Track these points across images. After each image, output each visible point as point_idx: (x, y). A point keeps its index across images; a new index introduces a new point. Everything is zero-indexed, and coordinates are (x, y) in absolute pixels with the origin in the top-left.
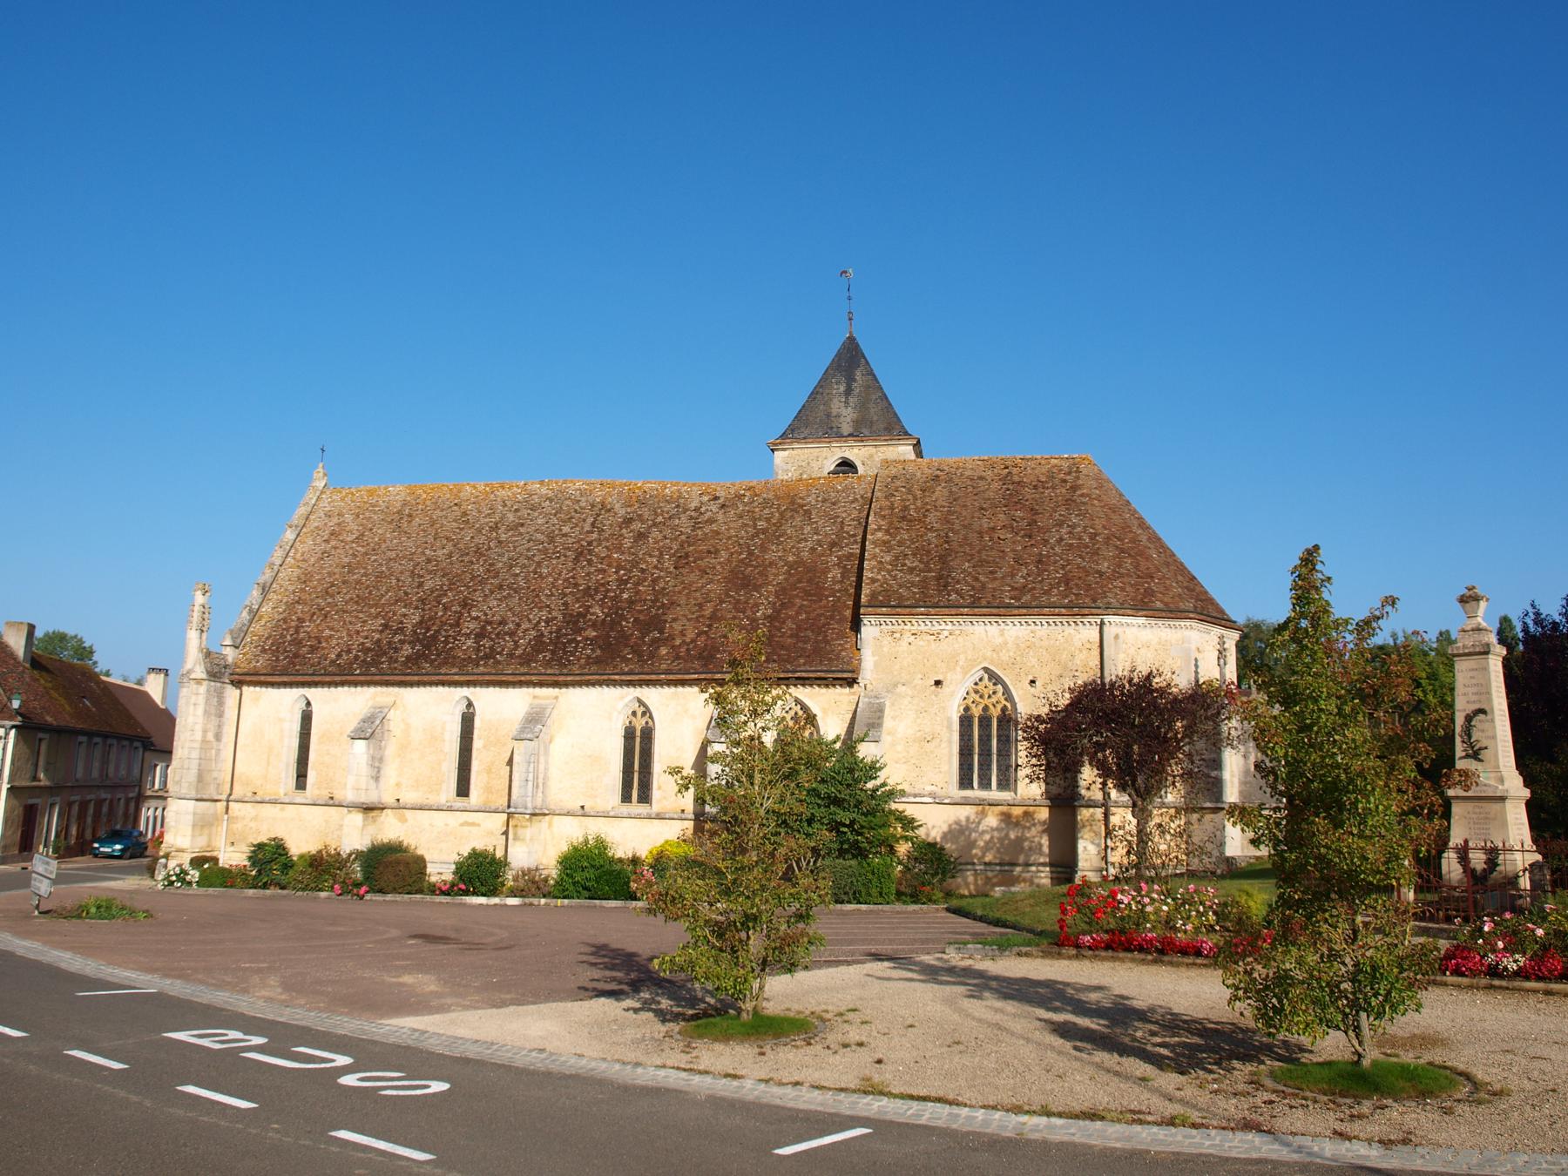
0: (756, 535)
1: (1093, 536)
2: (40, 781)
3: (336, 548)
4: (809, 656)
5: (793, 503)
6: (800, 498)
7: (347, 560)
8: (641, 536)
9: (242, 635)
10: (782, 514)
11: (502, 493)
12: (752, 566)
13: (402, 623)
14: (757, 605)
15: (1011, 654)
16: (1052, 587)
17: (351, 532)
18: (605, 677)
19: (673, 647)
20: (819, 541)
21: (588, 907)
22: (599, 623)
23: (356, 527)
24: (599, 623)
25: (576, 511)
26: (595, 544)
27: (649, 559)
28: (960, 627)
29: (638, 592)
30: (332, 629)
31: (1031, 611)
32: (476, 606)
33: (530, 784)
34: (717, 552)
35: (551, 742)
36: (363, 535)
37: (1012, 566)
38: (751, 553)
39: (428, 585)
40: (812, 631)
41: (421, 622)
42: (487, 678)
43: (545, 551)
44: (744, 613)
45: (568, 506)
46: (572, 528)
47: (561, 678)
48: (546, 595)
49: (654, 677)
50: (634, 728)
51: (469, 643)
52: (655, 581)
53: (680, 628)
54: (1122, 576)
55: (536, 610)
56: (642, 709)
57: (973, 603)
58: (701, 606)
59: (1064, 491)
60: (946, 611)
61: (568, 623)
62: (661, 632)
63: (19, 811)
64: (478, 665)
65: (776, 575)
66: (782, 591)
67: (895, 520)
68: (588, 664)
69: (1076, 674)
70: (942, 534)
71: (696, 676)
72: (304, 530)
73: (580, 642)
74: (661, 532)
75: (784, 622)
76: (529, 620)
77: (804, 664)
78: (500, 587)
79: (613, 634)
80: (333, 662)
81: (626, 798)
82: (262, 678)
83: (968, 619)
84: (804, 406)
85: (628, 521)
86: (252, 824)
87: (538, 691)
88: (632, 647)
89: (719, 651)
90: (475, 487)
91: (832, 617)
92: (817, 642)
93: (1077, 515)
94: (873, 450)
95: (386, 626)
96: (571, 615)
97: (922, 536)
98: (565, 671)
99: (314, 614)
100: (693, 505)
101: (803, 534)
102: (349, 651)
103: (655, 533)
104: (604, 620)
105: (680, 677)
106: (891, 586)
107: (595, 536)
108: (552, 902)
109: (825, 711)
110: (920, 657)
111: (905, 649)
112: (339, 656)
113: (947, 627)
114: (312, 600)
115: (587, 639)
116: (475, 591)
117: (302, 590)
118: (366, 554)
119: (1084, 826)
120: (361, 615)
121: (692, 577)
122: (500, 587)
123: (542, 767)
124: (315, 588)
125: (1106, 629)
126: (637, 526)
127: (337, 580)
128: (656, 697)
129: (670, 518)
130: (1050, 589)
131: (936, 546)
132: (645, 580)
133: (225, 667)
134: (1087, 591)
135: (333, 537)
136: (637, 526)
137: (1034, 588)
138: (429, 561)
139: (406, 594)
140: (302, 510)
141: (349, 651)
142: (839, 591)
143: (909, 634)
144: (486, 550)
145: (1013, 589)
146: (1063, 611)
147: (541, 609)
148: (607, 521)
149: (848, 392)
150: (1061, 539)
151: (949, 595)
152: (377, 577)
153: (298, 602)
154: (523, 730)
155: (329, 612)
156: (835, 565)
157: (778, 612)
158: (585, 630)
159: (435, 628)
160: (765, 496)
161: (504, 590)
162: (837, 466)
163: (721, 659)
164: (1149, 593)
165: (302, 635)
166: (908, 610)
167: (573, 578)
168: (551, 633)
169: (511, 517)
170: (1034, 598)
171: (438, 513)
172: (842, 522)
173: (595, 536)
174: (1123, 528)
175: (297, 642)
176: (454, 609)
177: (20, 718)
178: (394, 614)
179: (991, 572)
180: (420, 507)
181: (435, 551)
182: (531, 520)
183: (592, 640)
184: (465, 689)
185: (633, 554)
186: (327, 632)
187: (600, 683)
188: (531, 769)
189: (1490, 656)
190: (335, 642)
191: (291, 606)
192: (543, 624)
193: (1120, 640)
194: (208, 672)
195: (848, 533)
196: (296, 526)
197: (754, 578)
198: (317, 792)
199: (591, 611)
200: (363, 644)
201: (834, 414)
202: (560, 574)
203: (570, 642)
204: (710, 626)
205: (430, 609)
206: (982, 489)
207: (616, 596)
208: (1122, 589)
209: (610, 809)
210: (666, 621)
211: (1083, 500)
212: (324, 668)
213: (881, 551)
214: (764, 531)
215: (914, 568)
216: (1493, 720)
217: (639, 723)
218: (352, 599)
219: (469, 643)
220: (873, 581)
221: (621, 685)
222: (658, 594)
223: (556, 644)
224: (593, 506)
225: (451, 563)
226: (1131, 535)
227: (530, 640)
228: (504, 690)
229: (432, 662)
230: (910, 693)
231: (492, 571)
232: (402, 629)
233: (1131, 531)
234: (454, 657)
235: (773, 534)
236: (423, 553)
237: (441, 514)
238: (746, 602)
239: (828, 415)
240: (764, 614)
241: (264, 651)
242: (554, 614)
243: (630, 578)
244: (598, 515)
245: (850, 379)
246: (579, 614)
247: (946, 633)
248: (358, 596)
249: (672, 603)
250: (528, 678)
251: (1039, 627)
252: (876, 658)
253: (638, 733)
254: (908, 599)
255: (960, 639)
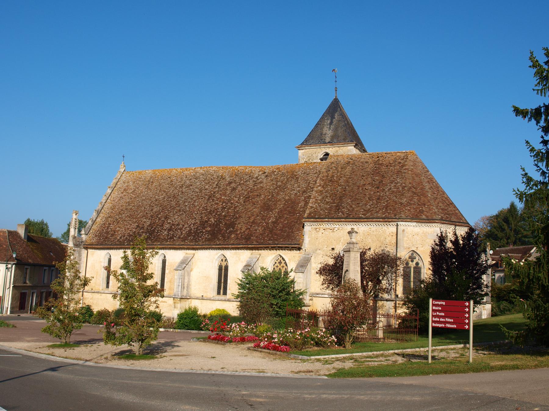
0: (276, 188)
1: (403, 188)
2: (27, 284)
3: (125, 195)
4: (284, 238)
5: (293, 174)
6: (296, 172)
7: (128, 200)
8: (234, 189)
9: (89, 230)
10: (288, 179)
11: (186, 172)
12: (272, 201)
13: (143, 225)
14: (270, 217)
15: (361, 237)
16: (380, 209)
17: (131, 189)
18: (210, 246)
19: (236, 234)
20: (299, 190)
21: (186, 332)
22: (212, 225)
23: (133, 187)
24: (212, 225)
25: (211, 179)
26: (216, 193)
27: (235, 199)
28: (342, 227)
29: (228, 212)
30: (119, 227)
31: (368, 220)
32: (170, 218)
33: (180, 287)
34: (261, 195)
35: (191, 271)
36: (135, 190)
37: (367, 201)
38: (273, 196)
39: (155, 210)
40: (288, 228)
41: (150, 225)
42: (169, 246)
43: (197, 196)
44: (264, 220)
45: (209, 177)
46: (209, 186)
47: (195, 247)
48: (195, 214)
49: (227, 246)
50: (222, 265)
51: (166, 233)
52: (235, 208)
53: (240, 227)
54: (411, 204)
55: (191, 220)
56: (225, 258)
57: (347, 216)
58: (249, 218)
59: (398, 167)
60: (336, 220)
61: (201, 225)
62: (233, 228)
63: (18, 295)
64: (167, 241)
65: (280, 205)
66: (281, 211)
67: (327, 181)
68: (205, 241)
69: (387, 246)
70: (344, 187)
71: (242, 246)
72: (115, 189)
73: (204, 232)
74: (241, 187)
75: (278, 224)
76: (188, 224)
77: (282, 241)
78: (180, 211)
79: (216, 229)
80: (118, 240)
81: (219, 293)
82: (94, 246)
83: (345, 223)
84: (312, 130)
85: (230, 183)
86: (91, 301)
87: (188, 251)
88: (222, 234)
89: (252, 236)
90: (177, 170)
91: (297, 222)
92: (289, 232)
93: (400, 178)
94: (338, 149)
95: (138, 226)
96: (203, 222)
97: (336, 188)
98: (197, 244)
99: (114, 221)
100: (255, 176)
101: (293, 188)
102: (124, 236)
103: (239, 188)
104: (214, 223)
105: (236, 246)
106: (318, 210)
107: (217, 189)
108: (175, 330)
109: (290, 260)
110: (326, 239)
111: (321, 235)
112: (121, 238)
113: (337, 227)
114: (114, 216)
115: (206, 231)
116: (170, 212)
117: (112, 212)
118: (135, 198)
119: (379, 308)
120: (130, 222)
121: (249, 206)
122: (180, 211)
123: (186, 281)
124: (116, 211)
125: (399, 227)
126: (233, 185)
127: (124, 208)
128: (229, 254)
129: (246, 181)
130: (379, 210)
131: (340, 193)
132: (232, 207)
133: (82, 242)
134: (394, 211)
135: (125, 191)
136: (233, 185)
137: (373, 210)
138: (156, 200)
139: (147, 213)
140: (115, 181)
141: (124, 236)
142: (301, 211)
143: (322, 229)
144: (177, 196)
145: (365, 210)
146: (381, 220)
147: (192, 219)
148: (223, 183)
149: (331, 123)
150: (390, 189)
151: (339, 213)
152: (138, 207)
153: (109, 217)
154: (179, 266)
155: (119, 221)
156: (303, 200)
157: (277, 220)
158: (207, 227)
159: (155, 227)
160: (283, 171)
161: (181, 212)
162: (324, 155)
163: (252, 239)
164: (422, 212)
165: (109, 230)
166: (321, 220)
167: (206, 206)
168: (194, 229)
169: (188, 182)
170: (372, 214)
171: (162, 181)
172: (309, 182)
173: (217, 189)
174: (419, 183)
175: (107, 233)
176: (162, 219)
177: (16, 261)
178: (141, 222)
179: (358, 204)
180: (156, 179)
181: (159, 196)
182: (195, 183)
183: (208, 231)
184: (163, 250)
185: (230, 197)
186: (118, 229)
187: (209, 249)
188: (181, 281)
189: (351, 252)
190: (120, 232)
191: (107, 218)
192: (192, 225)
193: (405, 232)
194: (74, 244)
195: (310, 187)
196: (112, 187)
197: (272, 206)
198: (112, 289)
199: (210, 220)
200: (129, 233)
201: (324, 133)
202: (201, 205)
203: (200, 232)
204: (251, 226)
205: (154, 219)
206: (365, 167)
207: (220, 214)
208: (409, 210)
209: (212, 297)
210: (236, 224)
211: (405, 171)
212: (115, 242)
213: (318, 195)
214: (280, 186)
215: (328, 202)
216: (349, 274)
217: (224, 264)
218: (128, 216)
219: (166, 233)
220: (312, 207)
221: (216, 249)
222: (235, 213)
223: (195, 233)
224: (218, 177)
225: (164, 201)
226: (421, 186)
227: (187, 232)
228: (176, 251)
229: (151, 240)
230: (322, 253)
231: (178, 204)
232: (143, 227)
233: (422, 185)
234: (160, 238)
235: (282, 188)
236: (155, 197)
237: (163, 181)
238: (267, 216)
239: (321, 134)
240: (272, 221)
241: (96, 236)
242: (197, 221)
243: (227, 206)
244: (219, 181)
245: (333, 117)
246: (206, 221)
247: (336, 229)
248: (130, 215)
249: (240, 217)
250: (183, 246)
251: (373, 227)
252: (310, 239)
253: (223, 268)
254: (323, 215)
255: (342, 231)
